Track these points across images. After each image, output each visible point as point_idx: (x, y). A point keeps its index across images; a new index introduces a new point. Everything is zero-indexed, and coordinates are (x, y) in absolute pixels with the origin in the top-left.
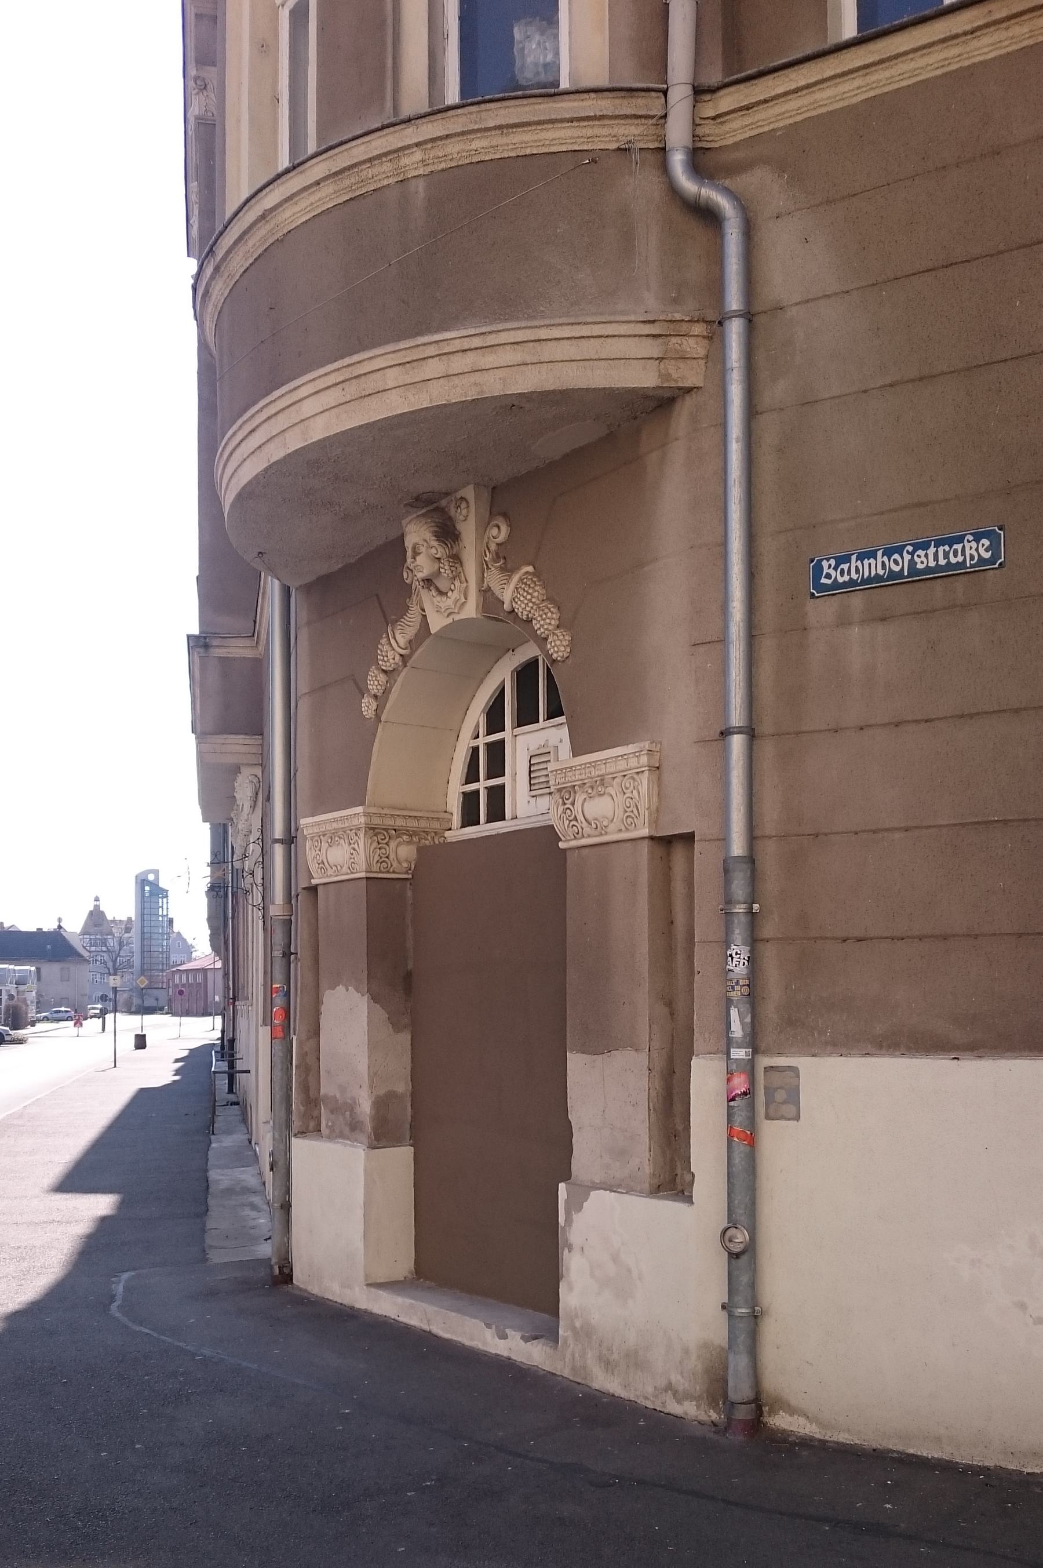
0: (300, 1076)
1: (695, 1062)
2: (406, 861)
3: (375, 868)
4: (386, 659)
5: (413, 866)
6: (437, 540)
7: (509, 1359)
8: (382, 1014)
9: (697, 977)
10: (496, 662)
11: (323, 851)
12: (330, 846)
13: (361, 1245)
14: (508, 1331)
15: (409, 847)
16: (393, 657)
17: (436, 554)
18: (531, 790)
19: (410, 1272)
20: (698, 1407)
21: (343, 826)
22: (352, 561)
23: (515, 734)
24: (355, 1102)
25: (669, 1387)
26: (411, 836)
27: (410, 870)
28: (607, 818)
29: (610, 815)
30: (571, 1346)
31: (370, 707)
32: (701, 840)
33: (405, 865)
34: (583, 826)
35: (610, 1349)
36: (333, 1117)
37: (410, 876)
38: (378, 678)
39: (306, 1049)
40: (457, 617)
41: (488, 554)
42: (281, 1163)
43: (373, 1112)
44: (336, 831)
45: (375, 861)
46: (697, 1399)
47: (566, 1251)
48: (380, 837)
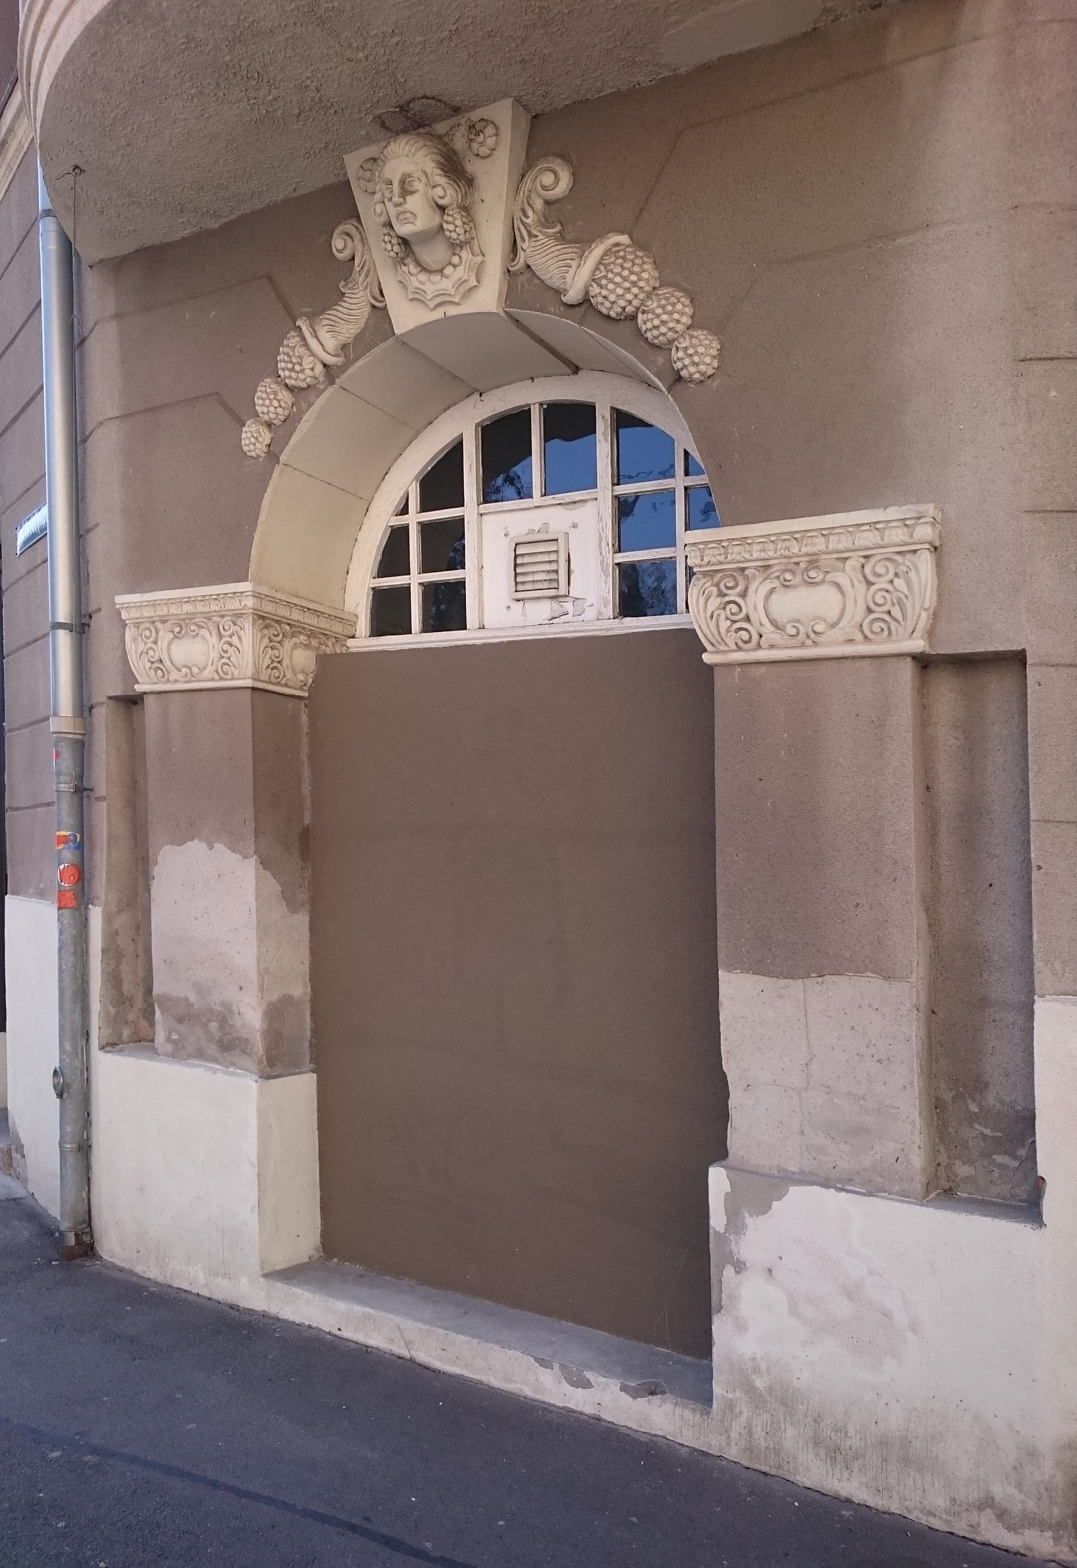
0: (108, 964)
1: (1041, 1007)
2: (303, 672)
3: (264, 676)
4: (298, 368)
5: (310, 681)
6: (446, 176)
7: (599, 1419)
8: (273, 886)
9: (1035, 875)
10: (445, 410)
11: (163, 643)
12: (176, 637)
13: (253, 1219)
14: (589, 1375)
15: (308, 652)
16: (311, 366)
17: (441, 198)
18: (516, 591)
19: (317, 1249)
20: (1057, 1540)
21: (206, 609)
22: (214, 225)
23: (481, 512)
24: (230, 1011)
25: (988, 1503)
26: (309, 637)
27: (305, 685)
28: (825, 621)
29: (833, 615)
30: (745, 1415)
31: (260, 439)
32: (1035, 665)
33: (301, 677)
34: (763, 630)
35: (841, 1430)
36: (182, 1028)
37: (306, 694)
38: (280, 397)
39: (116, 925)
40: (452, 311)
41: (530, 213)
42: (76, 1087)
43: (265, 1027)
44: (191, 616)
45: (265, 666)
46: (1057, 1527)
47: (729, 1272)
48: (272, 631)
